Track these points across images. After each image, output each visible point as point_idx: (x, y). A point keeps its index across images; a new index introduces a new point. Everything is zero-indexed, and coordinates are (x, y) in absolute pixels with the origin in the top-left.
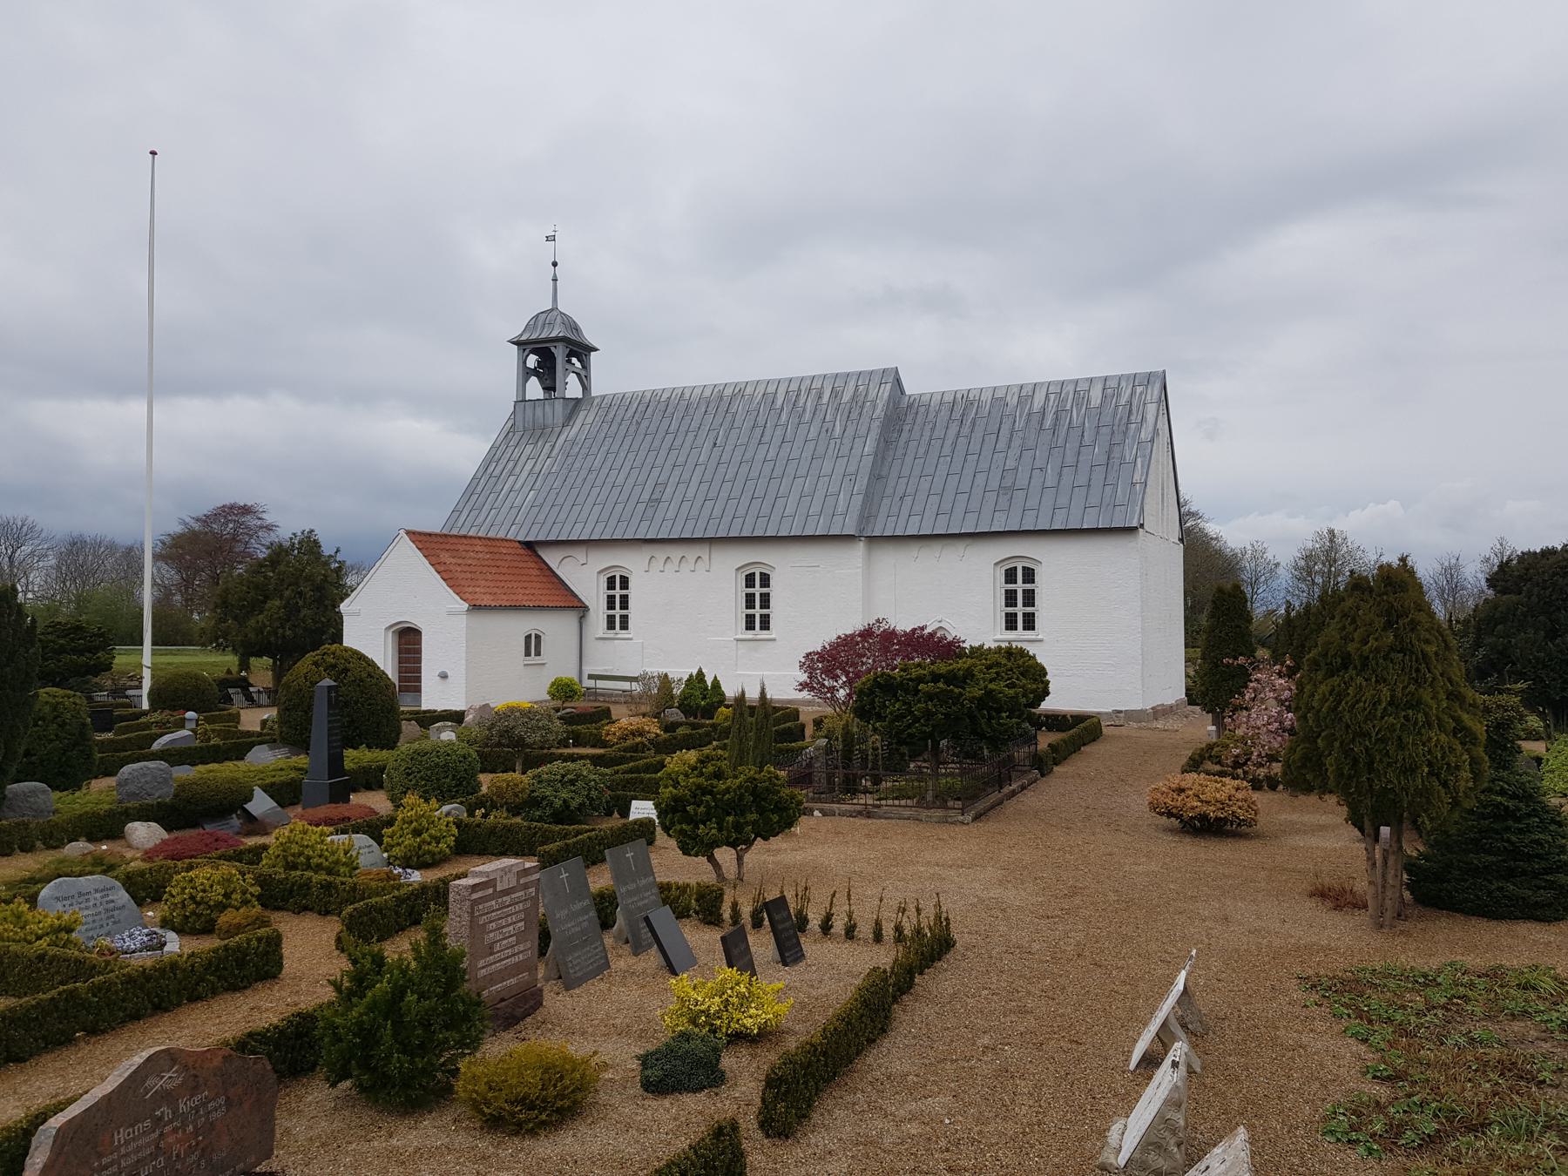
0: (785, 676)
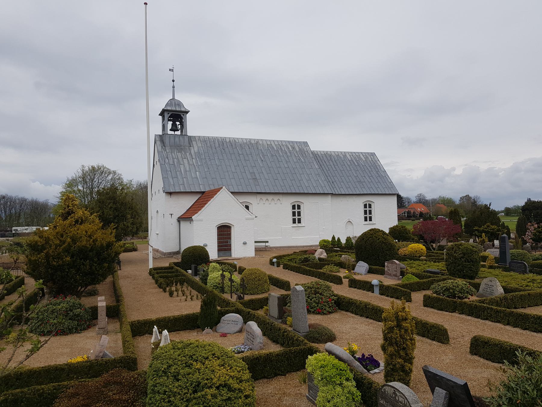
0: (309, 238)
